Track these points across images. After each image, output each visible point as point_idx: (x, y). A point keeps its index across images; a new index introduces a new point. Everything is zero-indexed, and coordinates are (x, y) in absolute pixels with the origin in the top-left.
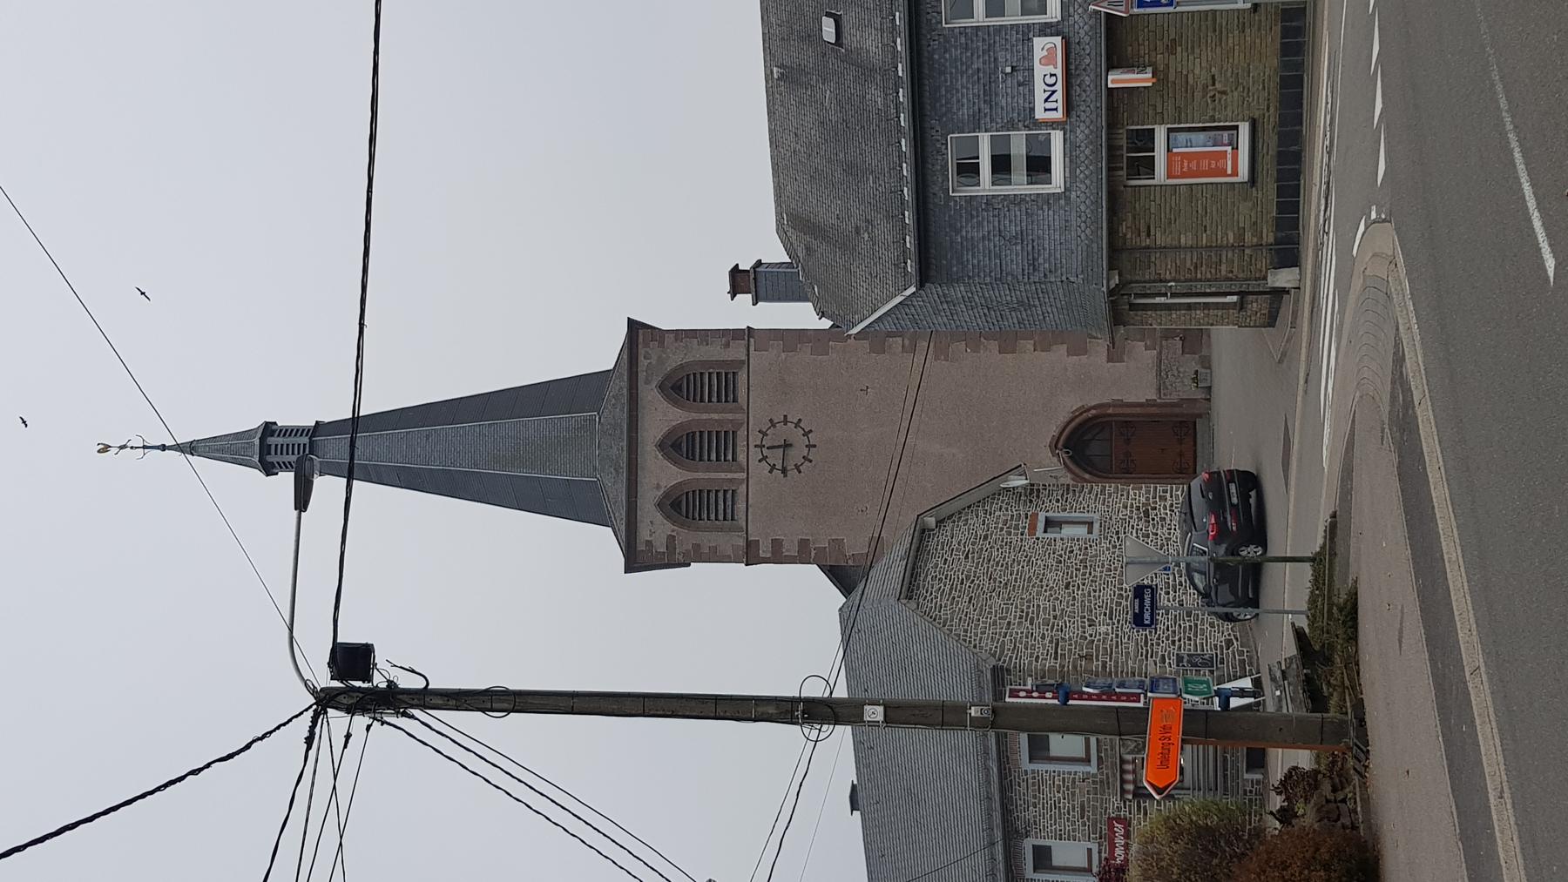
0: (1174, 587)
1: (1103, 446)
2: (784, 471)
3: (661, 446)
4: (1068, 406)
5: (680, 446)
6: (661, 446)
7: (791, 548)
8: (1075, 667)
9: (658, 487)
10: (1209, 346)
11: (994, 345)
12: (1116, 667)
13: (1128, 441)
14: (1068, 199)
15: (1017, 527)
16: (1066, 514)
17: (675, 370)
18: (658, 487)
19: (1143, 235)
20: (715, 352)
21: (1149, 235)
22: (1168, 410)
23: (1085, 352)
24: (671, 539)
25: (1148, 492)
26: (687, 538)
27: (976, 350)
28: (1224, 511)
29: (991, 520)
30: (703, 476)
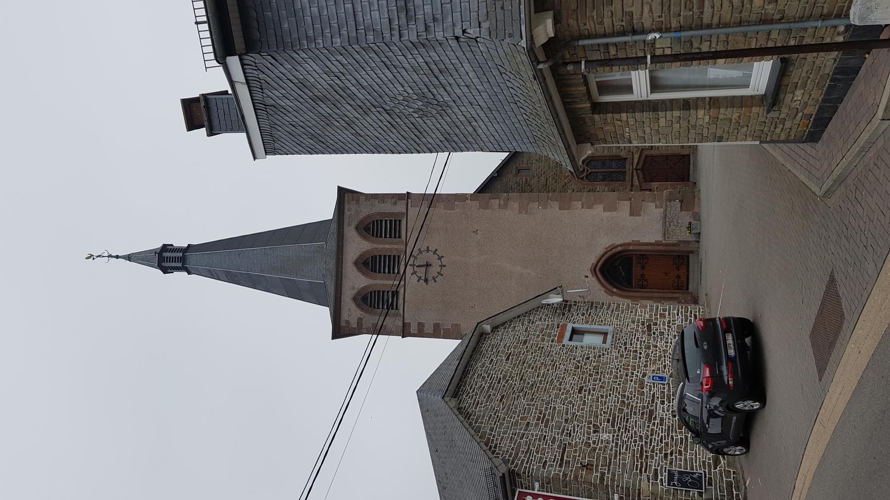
1: (621, 270)
2: (426, 280)
3: (356, 263)
4: (603, 243)
5: (369, 264)
6: (356, 263)
7: (429, 329)
8: (576, 477)
9: (353, 288)
10: (699, 206)
12: (613, 480)
13: (643, 268)
15: (549, 336)
17: (365, 218)
18: (353, 288)
20: (388, 208)
22: (671, 248)
23: (615, 209)
24: (360, 320)
25: (651, 310)
26: (370, 319)
27: (545, 207)
28: (720, 364)
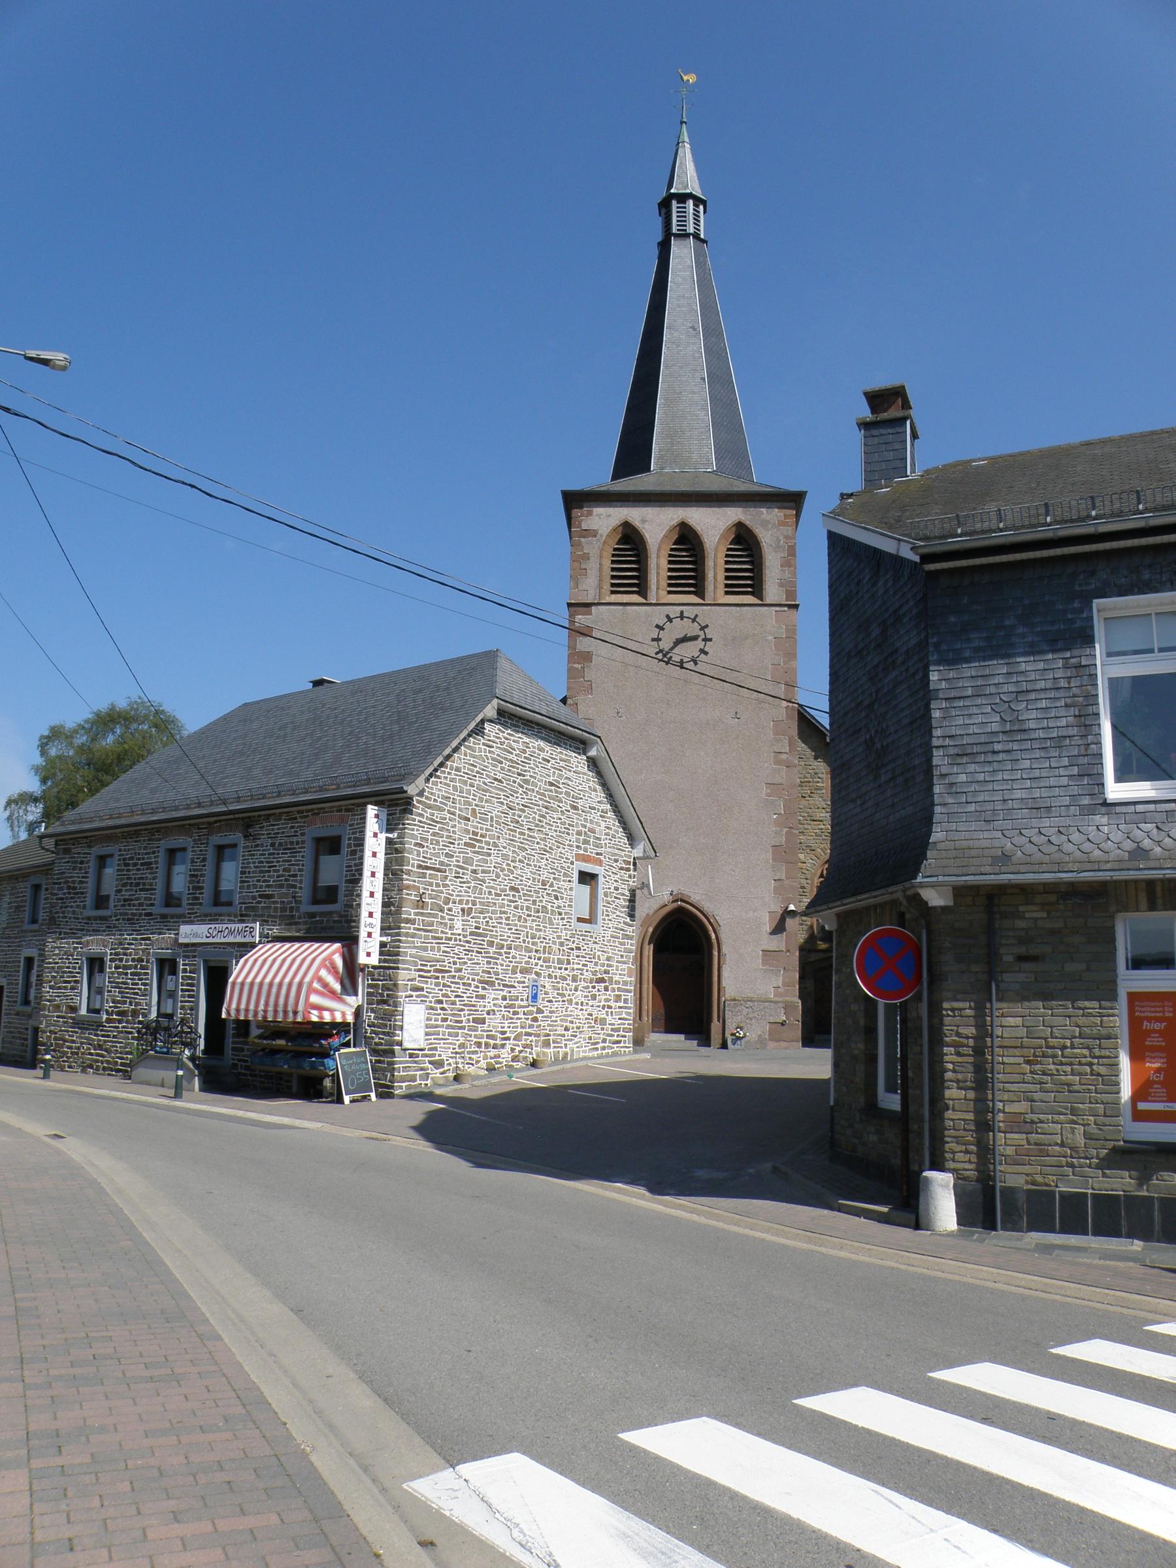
0: (511, 1006)
5: (687, 540)
9: (643, 521)
12: (407, 935)
14: (1090, 811)
15: (586, 842)
19: (1022, 950)
21: (1021, 959)
24: (593, 533)
25: (625, 983)
27: (777, 823)
29: (595, 816)
30: (658, 567)
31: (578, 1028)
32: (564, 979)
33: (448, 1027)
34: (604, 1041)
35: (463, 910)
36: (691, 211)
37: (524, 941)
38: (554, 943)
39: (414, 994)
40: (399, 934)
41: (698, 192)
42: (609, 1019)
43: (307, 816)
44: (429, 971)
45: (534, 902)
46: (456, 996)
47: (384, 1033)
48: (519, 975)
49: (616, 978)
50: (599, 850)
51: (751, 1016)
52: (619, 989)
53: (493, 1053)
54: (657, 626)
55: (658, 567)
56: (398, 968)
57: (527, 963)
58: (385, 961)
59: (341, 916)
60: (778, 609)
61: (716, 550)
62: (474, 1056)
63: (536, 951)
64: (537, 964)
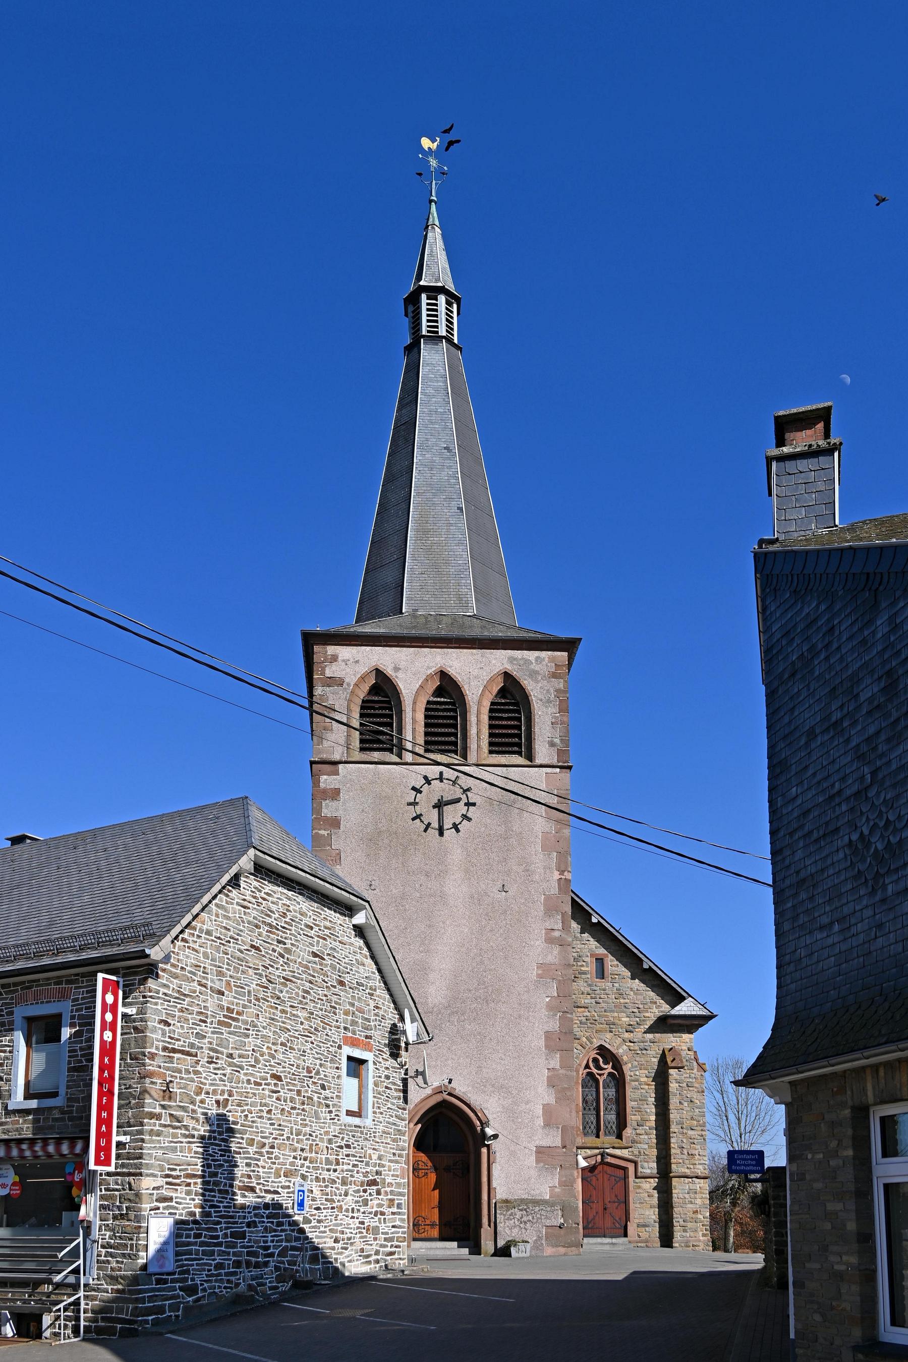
9: (397, 669)
11: (554, 1025)
16: (371, 1086)
18: (397, 669)
23: (547, 1125)
25: (398, 1185)
30: (413, 726)
31: (349, 1239)
32: (334, 1182)
33: (202, 1244)
34: (377, 1253)
35: (218, 1102)
36: (444, 310)
37: (288, 1138)
38: (322, 1140)
39: (161, 1205)
40: (140, 1132)
41: (451, 287)
42: (383, 1227)
43: (17, 991)
44: (178, 1177)
45: (299, 1092)
46: (212, 1206)
47: (124, 1255)
48: (283, 1179)
49: (389, 1180)
50: (369, 1033)
51: (525, 1219)
52: (392, 1192)
53: (255, 1272)
54: (414, 789)
55: (413, 726)
56: (141, 1174)
57: (292, 1164)
58: (123, 1166)
59: (63, 1112)
60: (549, 770)
61: (479, 703)
62: (233, 1278)
63: (302, 1150)
64: (302, 1166)
